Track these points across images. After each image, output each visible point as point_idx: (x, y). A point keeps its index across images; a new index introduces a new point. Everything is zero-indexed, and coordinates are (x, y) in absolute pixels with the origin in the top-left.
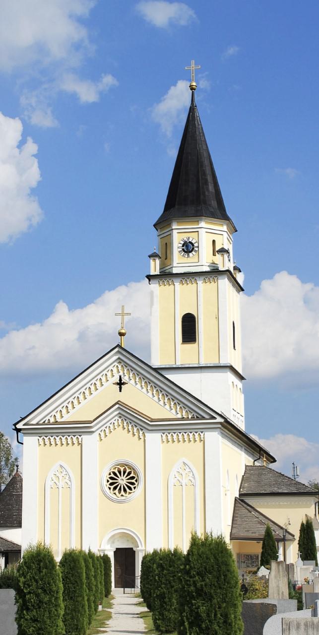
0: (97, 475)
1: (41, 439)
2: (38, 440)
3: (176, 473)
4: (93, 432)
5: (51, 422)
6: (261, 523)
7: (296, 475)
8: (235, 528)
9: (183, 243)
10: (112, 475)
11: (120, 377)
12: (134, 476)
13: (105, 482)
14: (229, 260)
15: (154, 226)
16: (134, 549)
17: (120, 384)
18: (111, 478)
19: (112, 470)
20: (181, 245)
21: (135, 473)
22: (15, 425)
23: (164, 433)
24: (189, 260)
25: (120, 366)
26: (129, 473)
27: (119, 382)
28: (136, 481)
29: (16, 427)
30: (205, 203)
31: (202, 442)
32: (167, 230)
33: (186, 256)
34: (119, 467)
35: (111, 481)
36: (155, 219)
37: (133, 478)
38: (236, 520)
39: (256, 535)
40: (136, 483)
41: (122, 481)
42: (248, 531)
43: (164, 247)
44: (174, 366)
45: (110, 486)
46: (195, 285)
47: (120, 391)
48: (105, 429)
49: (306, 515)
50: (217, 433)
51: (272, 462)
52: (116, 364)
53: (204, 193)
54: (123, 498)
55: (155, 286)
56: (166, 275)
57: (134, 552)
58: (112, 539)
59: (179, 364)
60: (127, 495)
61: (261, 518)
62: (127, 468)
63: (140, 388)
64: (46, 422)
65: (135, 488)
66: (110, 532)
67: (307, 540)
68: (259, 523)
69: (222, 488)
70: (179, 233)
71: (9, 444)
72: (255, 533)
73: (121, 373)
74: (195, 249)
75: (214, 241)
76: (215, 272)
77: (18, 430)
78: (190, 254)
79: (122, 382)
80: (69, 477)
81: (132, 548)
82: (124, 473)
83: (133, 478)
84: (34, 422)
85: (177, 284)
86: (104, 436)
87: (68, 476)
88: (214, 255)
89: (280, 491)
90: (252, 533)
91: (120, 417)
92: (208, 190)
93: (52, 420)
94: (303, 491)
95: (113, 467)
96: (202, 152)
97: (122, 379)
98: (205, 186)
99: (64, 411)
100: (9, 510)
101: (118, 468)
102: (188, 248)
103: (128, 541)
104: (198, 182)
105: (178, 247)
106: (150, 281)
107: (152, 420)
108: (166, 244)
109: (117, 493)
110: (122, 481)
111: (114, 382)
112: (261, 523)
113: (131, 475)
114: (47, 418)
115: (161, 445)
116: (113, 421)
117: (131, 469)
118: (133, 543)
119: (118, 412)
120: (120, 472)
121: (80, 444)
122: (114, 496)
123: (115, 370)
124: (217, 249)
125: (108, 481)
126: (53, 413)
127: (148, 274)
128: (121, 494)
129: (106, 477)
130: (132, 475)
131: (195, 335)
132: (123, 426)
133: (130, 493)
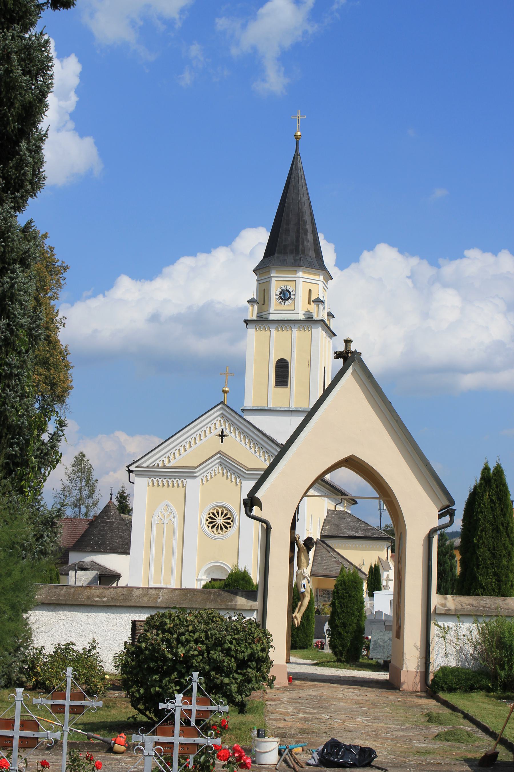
0: (198, 517)
1: (150, 480)
4: (196, 477)
5: (160, 466)
6: (338, 563)
7: (382, 509)
8: (315, 566)
10: (211, 515)
11: (222, 430)
13: (205, 521)
14: (324, 308)
15: (254, 271)
18: (210, 518)
19: (211, 511)
20: (279, 293)
22: (128, 467)
24: (285, 308)
25: (222, 421)
26: (226, 515)
28: (232, 521)
29: (129, 469)
30: (303, 252)
32: (266, 277)
33: (283, 304)
34: (217, 508)
35: (210, 520)
36: (255, 264)
37: (229, 518)
38: (317, 559)
39: (333, 573)
41: (220, 520)
42: (326, 569)
43: (263, 292)
44: (266, 408)
46: (290, 332)
47: (222, 442)
49: (261, 510)
51: (353, 504)
52: (219, 418)
53: (303, 243)
54: (220, 535)
55: (252, 332)
56: (262, 321)
59: (271, 406)
60: (223, 533)
61: (339, 558)
62: (224, 510)
63: (239, 441)
64: (155, 466)
65: (230, 527)
67: (374, 580)
68: (336, 562)
69: (305, 531)
70: (277, 281)
71: (90, 465)
72: (332, 571)
73: (223, 427)
74: (292, 297)
75: (310, 290)
76: (309, 321)
77: (130, 471)
78: (287, 302)
80: (174, 515)
82: (222, 514)
83: (229, 518)
84: (145, 465)
85: (273, 331)
88: (310, 303)
89: (357, 535)
90: (330, 571)
91: (221, 465)
92: (307, 240)
93: (161, 464)
94: (377, 536)
95: (212, 508)
96: (303, 201)
98: (304, 237)
99: (172, 457)
100: (103, 536)
102: (285, 296)
103: (222, 572)
104: (298, 231)
105: (276, 295)
106: (247, 324)
107: (249, 470)
108: (265, 289)
109: (215, 531)
110: (220, 520)
112: (338, 563)
113: (228, 516)
114: (156, 463)
116: (214, 468)
119: (219, 461)
120: (218, 513)
121: (184, 487)
122: (212, 534)
123: (218, 424)
124: (313, 298)
125: (207, 520)
126: (162, 458)
127: (246, 319)
129: (205, 516)
131: (288, 374)
132: (223, 473)
133: (226, 532)
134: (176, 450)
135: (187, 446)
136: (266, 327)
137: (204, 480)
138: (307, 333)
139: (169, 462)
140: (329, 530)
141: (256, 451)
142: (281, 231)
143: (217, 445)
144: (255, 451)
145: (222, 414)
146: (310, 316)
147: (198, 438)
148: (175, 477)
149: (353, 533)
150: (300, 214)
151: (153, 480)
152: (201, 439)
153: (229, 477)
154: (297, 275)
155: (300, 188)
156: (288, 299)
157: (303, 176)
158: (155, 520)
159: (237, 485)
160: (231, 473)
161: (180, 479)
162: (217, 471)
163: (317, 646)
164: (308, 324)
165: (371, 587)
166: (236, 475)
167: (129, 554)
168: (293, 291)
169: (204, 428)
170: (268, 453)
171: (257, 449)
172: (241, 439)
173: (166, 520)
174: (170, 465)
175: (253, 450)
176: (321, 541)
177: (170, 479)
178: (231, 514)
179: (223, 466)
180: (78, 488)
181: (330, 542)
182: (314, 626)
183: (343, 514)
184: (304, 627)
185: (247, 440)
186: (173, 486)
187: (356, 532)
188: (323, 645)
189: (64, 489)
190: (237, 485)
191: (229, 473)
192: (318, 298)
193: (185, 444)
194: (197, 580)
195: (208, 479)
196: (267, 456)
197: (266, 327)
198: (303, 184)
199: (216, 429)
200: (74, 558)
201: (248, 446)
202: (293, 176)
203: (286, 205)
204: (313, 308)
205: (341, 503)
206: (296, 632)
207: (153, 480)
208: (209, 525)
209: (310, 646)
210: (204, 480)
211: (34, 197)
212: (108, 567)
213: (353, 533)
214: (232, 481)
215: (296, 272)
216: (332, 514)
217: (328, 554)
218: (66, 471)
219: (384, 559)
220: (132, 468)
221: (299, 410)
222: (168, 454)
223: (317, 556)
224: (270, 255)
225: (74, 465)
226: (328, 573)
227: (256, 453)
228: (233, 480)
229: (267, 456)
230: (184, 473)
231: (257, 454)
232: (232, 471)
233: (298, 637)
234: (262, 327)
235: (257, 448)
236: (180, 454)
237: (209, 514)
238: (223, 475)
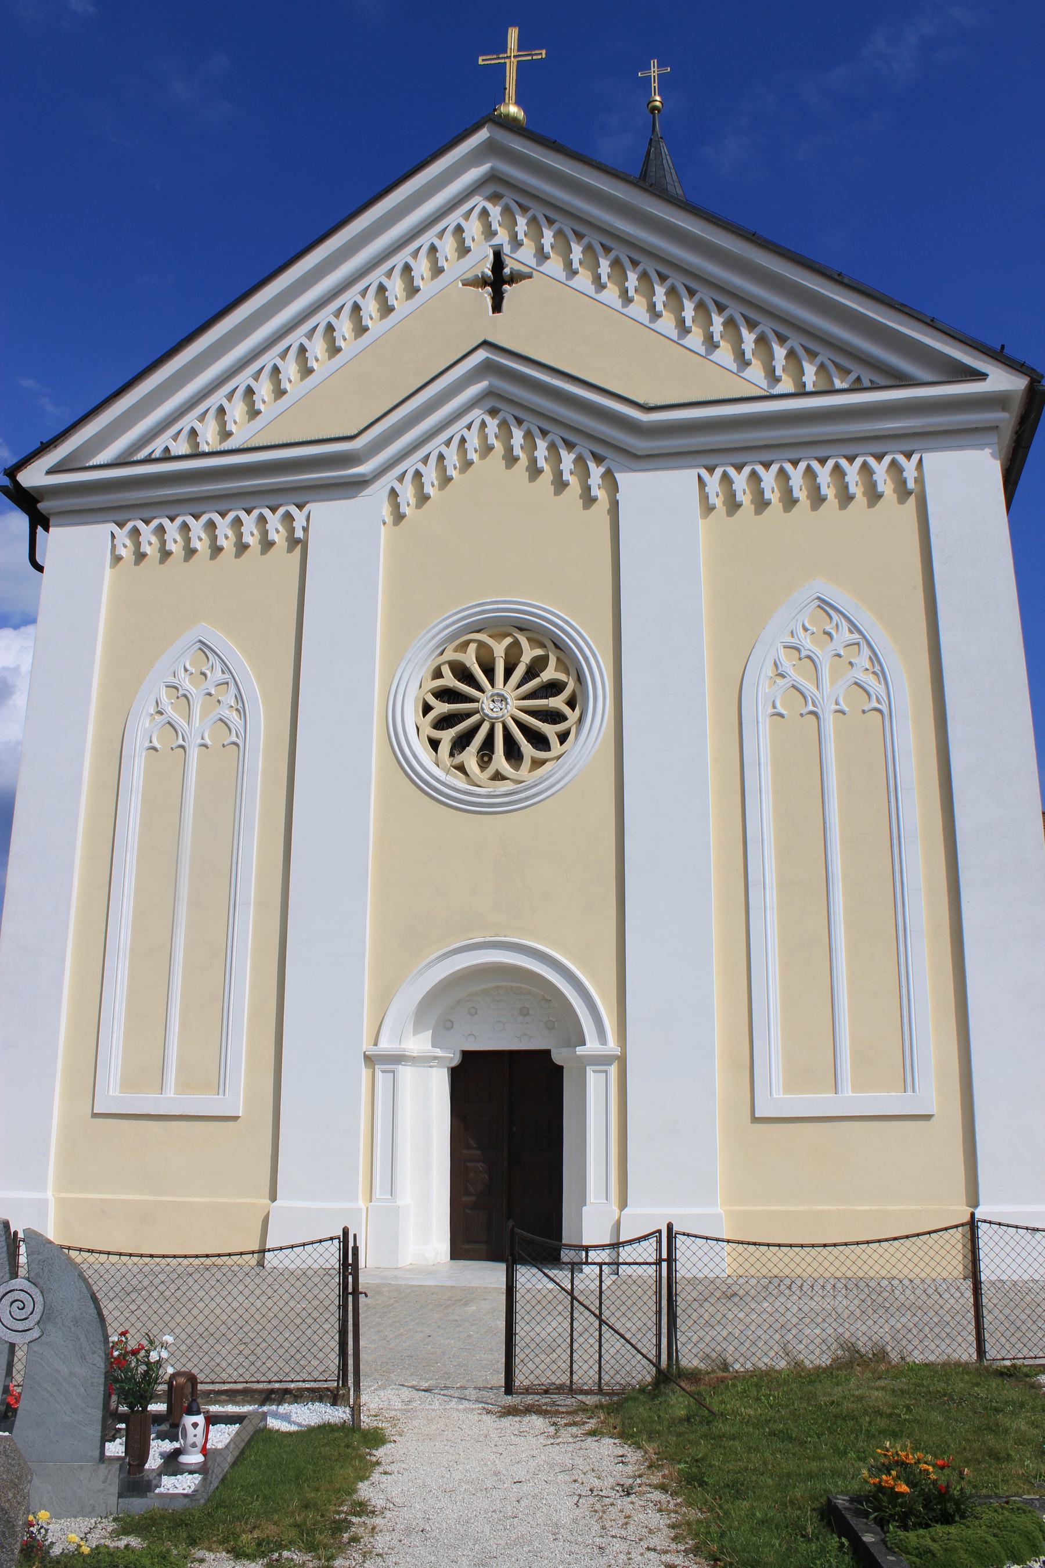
0: (373, 684)
1: (122, 535)
2: (113, 536)
3: (782, 651)
10: (449, 680)
12: (563, 677)
13: (411, 714)
16: (557, 1058)
17: (498, 280)
19: (450, 655)
21: (562, 665)
23: (711, 470)
25: (495, 212)
28: (571, 703)
31: (912, 500)
34: (482, 637)
35: (442, 708)
37: (553, 688)
40: (572, 716)
41: (502, 703)
45: (436, 734)
47: (497, 307)
48: (465, 432)
50: (987, 451)
57: (558, 1071)
58: (444, 1004)
65: (563, 737)
66: (429, 966)
73: (502, 237)
79: (507, 271)
80: (875, 658)
81: (547, 1053)
83: (553, 688)
86: (412, 501)
87: (866, 651)
97: (507, 261)
101: (481, 645)
103: (524, 1012)
110: (502, 703)
111: (469, 275)
115: (702, 525)
117: (543, 646)
118: (550, 1027)
121: (297, 543)
122: (458, 781)
123: (473, 228)
125: (427, 709)
126: (188, 421)
128: (491, 770)
129: (414, 685)
130: (549, 674)
133: (537, 764)
162: (473, 441)
178: (568, 661)
194: (370, 1060)
199: (464, 250)
208: (436, 734)
227: (655, 315)
231: (695, 339)
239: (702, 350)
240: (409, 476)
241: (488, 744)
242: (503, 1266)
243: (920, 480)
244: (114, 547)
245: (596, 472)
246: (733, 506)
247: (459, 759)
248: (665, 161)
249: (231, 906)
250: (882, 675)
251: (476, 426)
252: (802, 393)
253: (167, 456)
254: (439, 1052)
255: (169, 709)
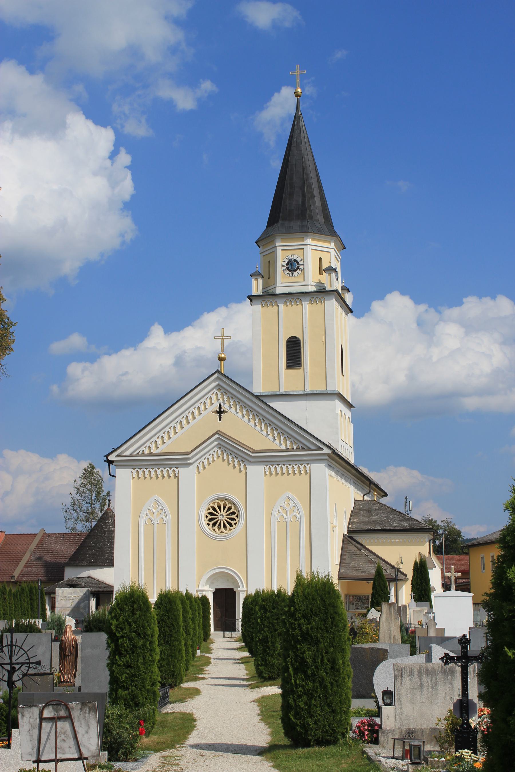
0: (195, 513)
1: (134, 472)
6: (371, 562)
7: (408, 510)
8: (344, 566)
9: (287, 261)
11: (220, 405)
13: (203, 517)
14: (337, 280)
16: (235, 590)
18: (210, 514)
19: (211, 505)
20: (285, 263)
22: (107, 456)
24: (294, 279)
25: (219, 394)
26: (229, 509)
27: (218, 410)
30: (311, 217)
31: (308, 474)
33: (291, 275)
34: (218, 501)
35: (210, 517)
37: (233, 513)
38: (345, 559)
39: (366, 575)
41: (222, 516)
44: (278, 393)
45: (209, 522)
47: (220, 420)
51: (383, 496)
52: (215, 391)
54: (223, 535)
58: (212, 579)
59: (283, 390)
60: (227, 531)
61: (371, 556)
63: (241, 417)
64: (140, 453)
65: (235, 524)
67: (421, 580)
68: (369, 561)
69: (329, 524)
70: (282, 251)
71: (100, 477)
72: (365, 572)
73: (221, 401)
75: (320, 259)
77: (110, 462)
78: (295, 273)
79: (222, 410)
80: (165, 513)
82: (224, 508)
83: (233, 513)
84: (127, 453)
85: (281, 306)
88: (321, 273)
89: (392, 527)
90: (362, 572)
91: (220, 448)
92: (314, 204)
93: (147, 451)
94: (416, 527)
95: (211, 501)
96: (307, 162)
99: (160, 442)
102: (293, 266)
103: (228, 581)
104: (303, 195)
106: (251, 301)
107: (254, 452)
108: (269, 262)
109: (217, 530)
110: (222, 516)
111: (213, 410)
112: (371, 562)
114: (141, 450)
119: (217, 443)
120: (219, 508)
121: (177, 477)
123: (214, 398)
125: (207, 517)
126: (148, 444)
128: (220, 531)
129: (204, 512)
133: (230, 530)
134: (164, 433)
135: (178, 427)
136: (273, 302)
137: (201, 467)
138: (320, 306)
139: (157, 448)
140: (357, 523)
141: (263, 429)
142: (284, 196)
143: (214, 424)
144: (261, 428)
145: (218, 385)
146: (322, 288)
147: (190, 417)
148: (165, 466)
149: (387, 525)
150: (304, 177)
151: (137, 472)
152: (194, 418)
153: (231, 462)
154: (305, 243)
155: (303, 148)
156: (296, 270)
157: (306, 136)
158: (143, 520)
159: (241, 471)
160: (233, 458)
161: (171, 468)
162: (215, 455)
163: (361, 734)
164: (320, 296)
165: (418, 589)
166: (240, 458)
167: (111, 564)
168: (302, 260)
169: (198, 404)
170: (277, 430)
171: (263, 426)
172: (243, 415)
173: (156, 520)
174: (157, 451)
175: (258, 428)
176: (349, 537)
177: (159, 469)
178: (236, 508)
179: (223, 449)
180: (88, 501)
181: (359, 538)
182: (350, 684)
183: (373, 504)
184: (325, 687)
185: (251, 415)
186: (163, 477)
187: (390, 524)
188: (377, 732)
189: (74, 503)
190: (241, 471)
191: (230, 457)
192: (330, 267)
193: (175, 425)
195: (206, 466)
196: (276, 433)
197: (273, 302)
198: (307, 144)
199: (212, 404)
200: (69, 573)
201: (252, 423)
202: (295, 136)
203: (289, 167)
204: (325, 278)
205: (369, 493)
206: (306, 704)
207: (137, 472)
208: (209, 522)
209: (343, 735)
210: (201, 467)
211: (316, 573)
212: (107, 583)
213: (387, 525)
214: (234, 467)
215: (303, 239)
216: (360, 505)
217: (359, 552)
218: (75, 484)
219: (427, 555)
220: (111, 458)
221: (315, 392)
222: (155, 438)
223: (345, 555)
224: (273, 224)
225: (83, 478)
226: (359, 574)
227: (262, 430)
228: (236, 465)
229: (276, 433)
230: (176, 460)
231: (264, 432)
232: (233, 455)
233: (311, 716)
234: (269, 303)
235: (263, 424)
236: (170, 438)
237: (209, 509)
238: (224, 460)
239: (266, 435)
240: (201, 463)
241: (220, 524)
242: (223, 632)
243: (310, 470)
244: (132, 475)
245: (242, 464)
246: (271, 474)
247: (214, 528)
248: (302, 130)
249: (166, 560)
250: (299, 513)
251: (216, 451)
252: (287, 450)
253: (143, 455)
254: (211, 589)
255: (149, 515)
